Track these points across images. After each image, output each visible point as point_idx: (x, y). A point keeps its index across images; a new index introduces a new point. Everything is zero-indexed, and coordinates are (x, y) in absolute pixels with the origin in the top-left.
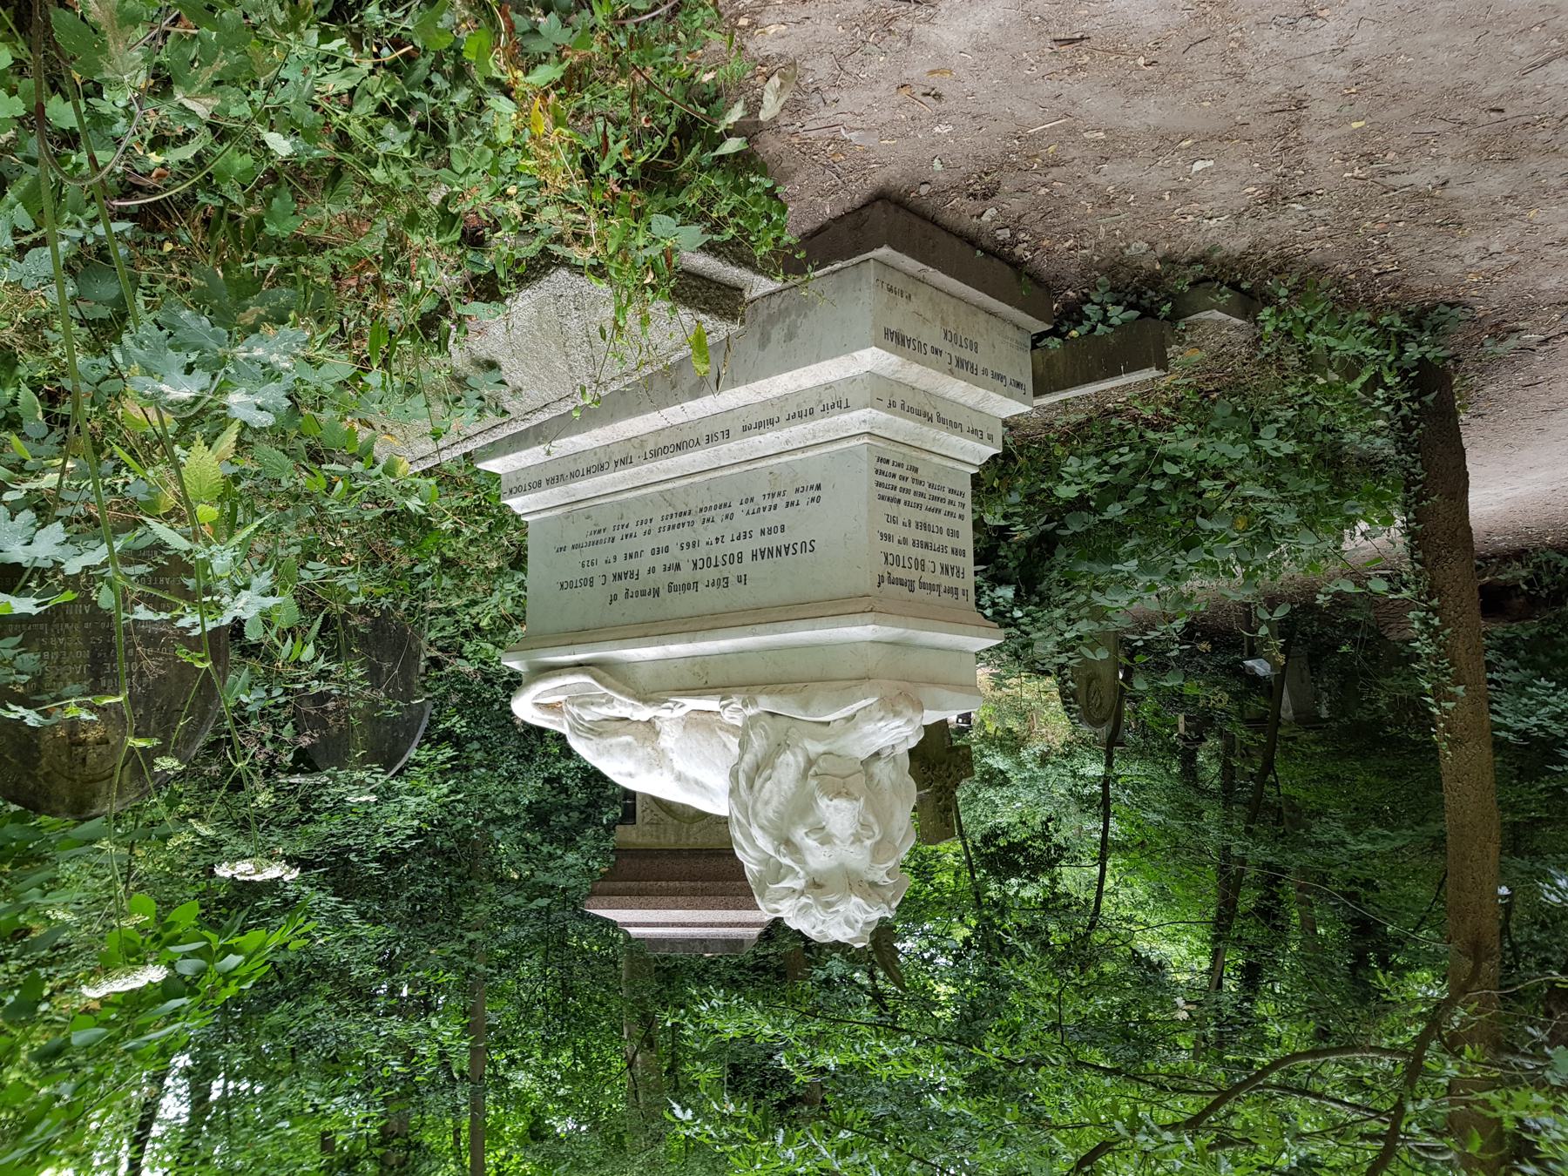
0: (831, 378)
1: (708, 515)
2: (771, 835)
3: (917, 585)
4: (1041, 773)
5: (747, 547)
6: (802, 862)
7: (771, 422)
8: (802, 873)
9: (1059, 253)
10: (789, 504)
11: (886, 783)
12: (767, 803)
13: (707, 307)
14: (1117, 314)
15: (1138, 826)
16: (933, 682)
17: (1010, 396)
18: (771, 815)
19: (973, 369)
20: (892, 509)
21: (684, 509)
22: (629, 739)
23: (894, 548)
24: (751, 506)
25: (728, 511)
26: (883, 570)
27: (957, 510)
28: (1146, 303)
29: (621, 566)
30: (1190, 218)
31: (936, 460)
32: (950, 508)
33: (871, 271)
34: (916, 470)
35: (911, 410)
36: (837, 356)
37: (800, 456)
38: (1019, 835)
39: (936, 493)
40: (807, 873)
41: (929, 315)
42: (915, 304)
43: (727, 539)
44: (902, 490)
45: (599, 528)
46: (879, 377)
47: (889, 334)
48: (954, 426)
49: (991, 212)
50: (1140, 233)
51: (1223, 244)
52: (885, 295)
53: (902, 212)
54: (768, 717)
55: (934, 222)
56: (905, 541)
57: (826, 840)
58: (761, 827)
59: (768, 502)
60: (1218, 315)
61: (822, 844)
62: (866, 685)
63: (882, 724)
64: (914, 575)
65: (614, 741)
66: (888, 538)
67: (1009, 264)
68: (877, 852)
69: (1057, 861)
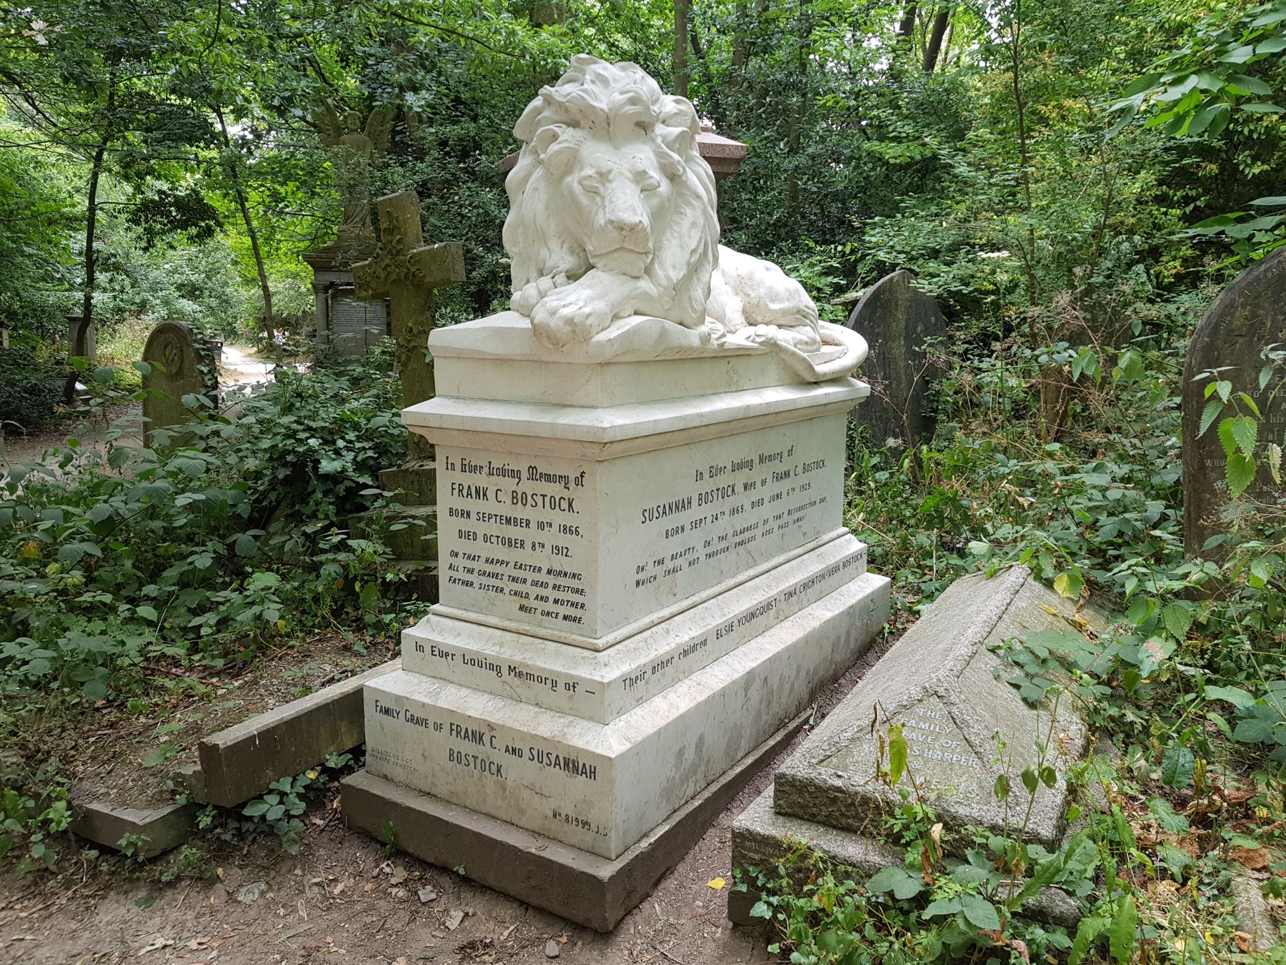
0: (638, 711)
1: (723, 545)
2: (689, 188)
3: (525, 475)
4: (147, 295)
5: (695, 512)
6: (659, 154)
7: (685, 653)
8: (659, 141)
9: (346, 873)
10: (661, 562)
11: (554, 245)
12: (694, 224)
13: (832, 794)
14: (271, 809)
15: (50, 242)
16: (502, 361)
17: (399, 699)
18: (688, 211)
19: (456, 730)
20: (559, 563)
21: (741, 549)
22: (774, 306)
23: (559, 518)
24: (690, 557)
25: (709, 550)
26: (575, 492)
27: (460, 562)
28: (232, 824)
29: (785, 484)
30: (193, 944)
31: (494, 621)
32: (470, 564)
33: (614, 845)
34: (522, 608)
35: (541, 680)
36: (644, 741)
37: (654, 617)
38: (179, 236)
39: (493, 582)
40: (653, 140)
41: (525, 794)
42: (547, 807)
43: (709, 519)
44: (544, 585)
45: (795, 528)
46: (591, 719)
47: (592, 773)
48: (473, 661)
49: (453, 923)
50: (253, 913)
51: (135, 909)
52: (594, 817)
53: (580, 919)
54: (687, 321)
55: (525, 905)
56: (541, 526)
57: (640, 176)
58: (698, 197)
59: (678, 562)
60: (130, 815)
61: (645, 172)
62: (608, 355)
63: (587, 310)
64: (527, 486)
65: (786, 305)
66: (565, 529)
67: (411, 856)
68: (572, 161)
69: (139, 210)
